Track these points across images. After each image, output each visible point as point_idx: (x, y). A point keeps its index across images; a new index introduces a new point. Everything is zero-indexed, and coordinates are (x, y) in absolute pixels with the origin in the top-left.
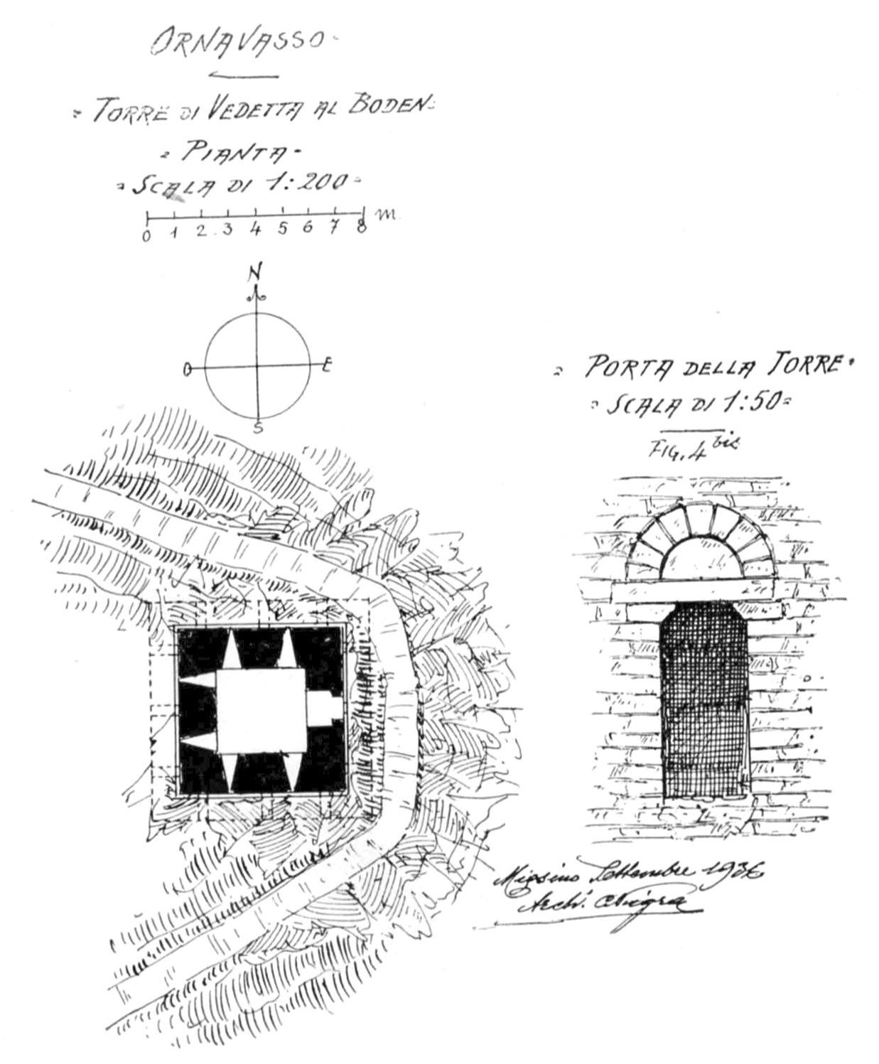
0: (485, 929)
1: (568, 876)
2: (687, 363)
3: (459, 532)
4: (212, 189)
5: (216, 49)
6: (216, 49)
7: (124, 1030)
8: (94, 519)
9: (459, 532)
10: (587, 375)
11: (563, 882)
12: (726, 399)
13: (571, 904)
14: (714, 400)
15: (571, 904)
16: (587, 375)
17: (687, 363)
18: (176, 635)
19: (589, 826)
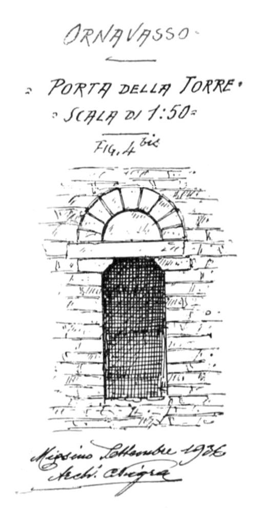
2: (122, 85)
13: (87, 475)
14: (141, 111)
15: (87, 475)
17: (122, 85)
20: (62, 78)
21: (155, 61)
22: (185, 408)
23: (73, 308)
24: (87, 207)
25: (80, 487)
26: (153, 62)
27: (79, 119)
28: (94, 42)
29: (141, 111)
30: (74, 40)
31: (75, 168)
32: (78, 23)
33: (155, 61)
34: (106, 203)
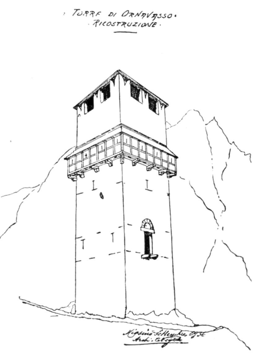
0: (57, 162)
1: (174, 334)
2: (75, 10)
3: (143, 102)
4: (127, 74)
5: (142, 147)
6: (142, 147)
7: (139, 26)
8: (76, 181)
9: (143, 102)
10: (203, 120)
11: (144, 335)
12: (93, 24)
13: (146, 340)
14: (73, 15)
15: (146, 340)
16: (203, 120)
17: (75, 10)
18: (106, 83)
19: (251, 280)
20: (83, 178)
21: (136, 252)
22: (105, 135)
23: (62, 310)
24: (137, 141)
25: (165, 257)
26: (137, 252)
27: (155, 249)
28: (140, 253)
29: (73, 15)
30: (194, 189)
31: (215, 242)
32: (160, 114)
33: (136, 252)
34: (114, 131)
